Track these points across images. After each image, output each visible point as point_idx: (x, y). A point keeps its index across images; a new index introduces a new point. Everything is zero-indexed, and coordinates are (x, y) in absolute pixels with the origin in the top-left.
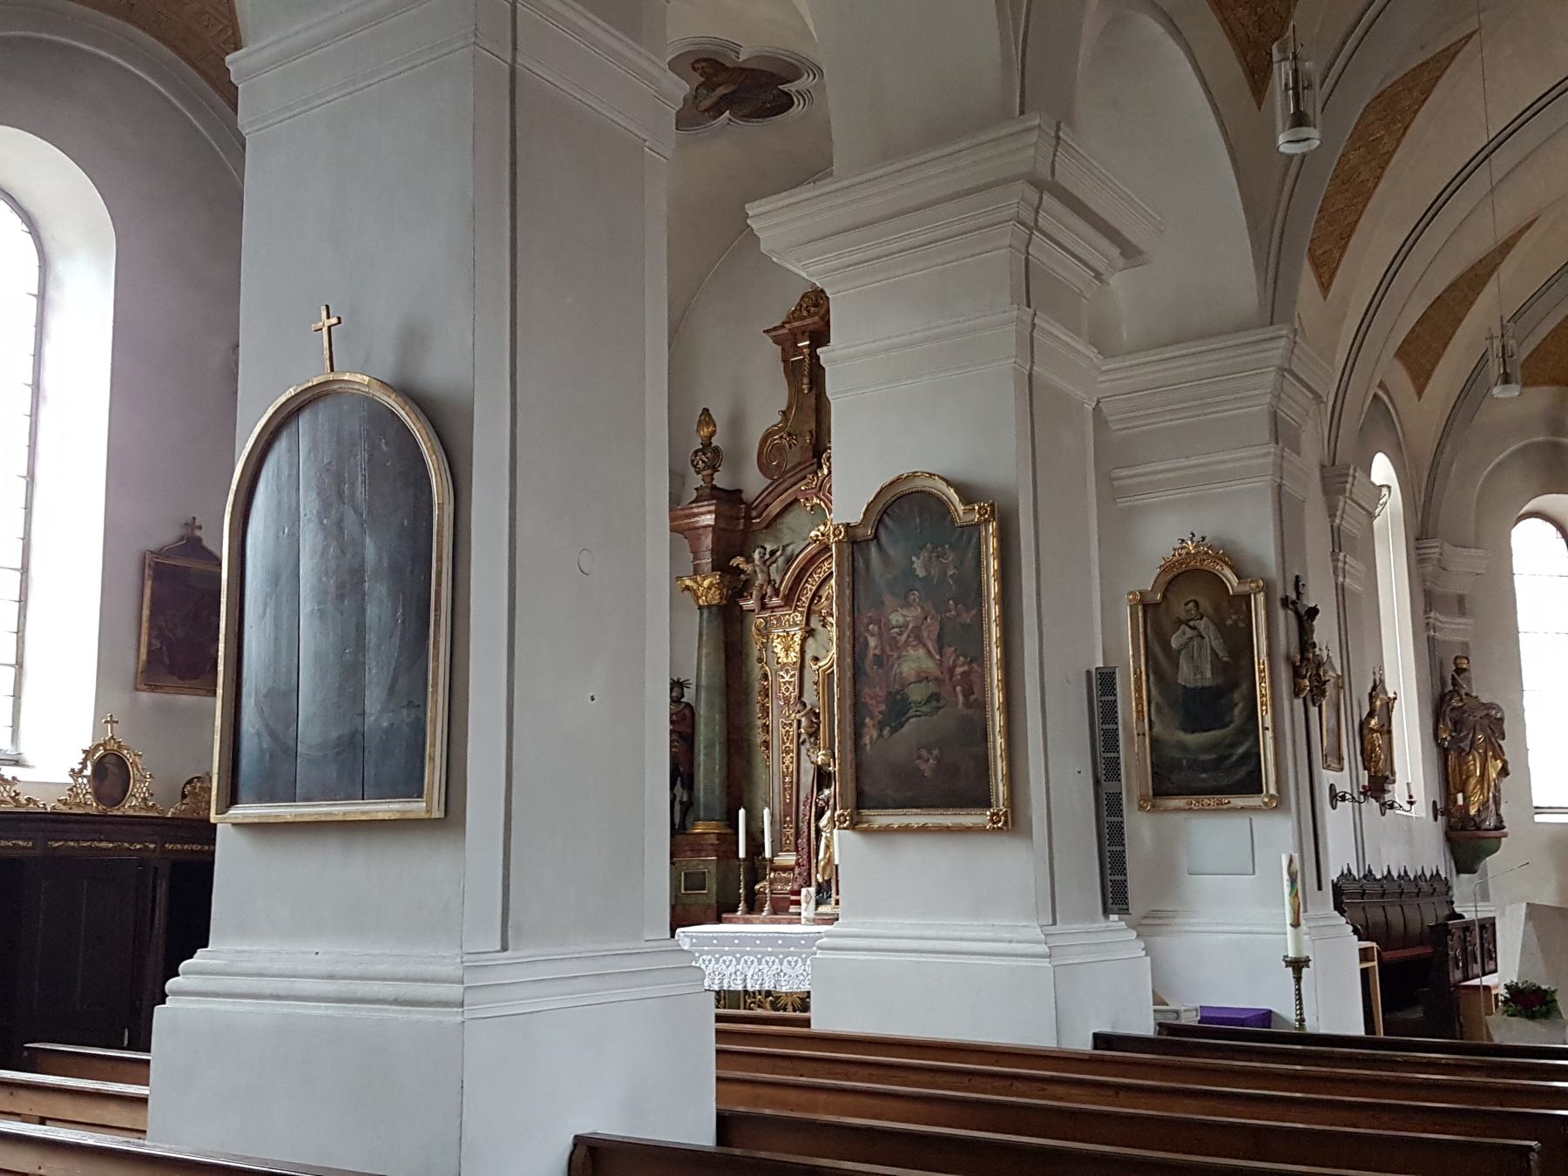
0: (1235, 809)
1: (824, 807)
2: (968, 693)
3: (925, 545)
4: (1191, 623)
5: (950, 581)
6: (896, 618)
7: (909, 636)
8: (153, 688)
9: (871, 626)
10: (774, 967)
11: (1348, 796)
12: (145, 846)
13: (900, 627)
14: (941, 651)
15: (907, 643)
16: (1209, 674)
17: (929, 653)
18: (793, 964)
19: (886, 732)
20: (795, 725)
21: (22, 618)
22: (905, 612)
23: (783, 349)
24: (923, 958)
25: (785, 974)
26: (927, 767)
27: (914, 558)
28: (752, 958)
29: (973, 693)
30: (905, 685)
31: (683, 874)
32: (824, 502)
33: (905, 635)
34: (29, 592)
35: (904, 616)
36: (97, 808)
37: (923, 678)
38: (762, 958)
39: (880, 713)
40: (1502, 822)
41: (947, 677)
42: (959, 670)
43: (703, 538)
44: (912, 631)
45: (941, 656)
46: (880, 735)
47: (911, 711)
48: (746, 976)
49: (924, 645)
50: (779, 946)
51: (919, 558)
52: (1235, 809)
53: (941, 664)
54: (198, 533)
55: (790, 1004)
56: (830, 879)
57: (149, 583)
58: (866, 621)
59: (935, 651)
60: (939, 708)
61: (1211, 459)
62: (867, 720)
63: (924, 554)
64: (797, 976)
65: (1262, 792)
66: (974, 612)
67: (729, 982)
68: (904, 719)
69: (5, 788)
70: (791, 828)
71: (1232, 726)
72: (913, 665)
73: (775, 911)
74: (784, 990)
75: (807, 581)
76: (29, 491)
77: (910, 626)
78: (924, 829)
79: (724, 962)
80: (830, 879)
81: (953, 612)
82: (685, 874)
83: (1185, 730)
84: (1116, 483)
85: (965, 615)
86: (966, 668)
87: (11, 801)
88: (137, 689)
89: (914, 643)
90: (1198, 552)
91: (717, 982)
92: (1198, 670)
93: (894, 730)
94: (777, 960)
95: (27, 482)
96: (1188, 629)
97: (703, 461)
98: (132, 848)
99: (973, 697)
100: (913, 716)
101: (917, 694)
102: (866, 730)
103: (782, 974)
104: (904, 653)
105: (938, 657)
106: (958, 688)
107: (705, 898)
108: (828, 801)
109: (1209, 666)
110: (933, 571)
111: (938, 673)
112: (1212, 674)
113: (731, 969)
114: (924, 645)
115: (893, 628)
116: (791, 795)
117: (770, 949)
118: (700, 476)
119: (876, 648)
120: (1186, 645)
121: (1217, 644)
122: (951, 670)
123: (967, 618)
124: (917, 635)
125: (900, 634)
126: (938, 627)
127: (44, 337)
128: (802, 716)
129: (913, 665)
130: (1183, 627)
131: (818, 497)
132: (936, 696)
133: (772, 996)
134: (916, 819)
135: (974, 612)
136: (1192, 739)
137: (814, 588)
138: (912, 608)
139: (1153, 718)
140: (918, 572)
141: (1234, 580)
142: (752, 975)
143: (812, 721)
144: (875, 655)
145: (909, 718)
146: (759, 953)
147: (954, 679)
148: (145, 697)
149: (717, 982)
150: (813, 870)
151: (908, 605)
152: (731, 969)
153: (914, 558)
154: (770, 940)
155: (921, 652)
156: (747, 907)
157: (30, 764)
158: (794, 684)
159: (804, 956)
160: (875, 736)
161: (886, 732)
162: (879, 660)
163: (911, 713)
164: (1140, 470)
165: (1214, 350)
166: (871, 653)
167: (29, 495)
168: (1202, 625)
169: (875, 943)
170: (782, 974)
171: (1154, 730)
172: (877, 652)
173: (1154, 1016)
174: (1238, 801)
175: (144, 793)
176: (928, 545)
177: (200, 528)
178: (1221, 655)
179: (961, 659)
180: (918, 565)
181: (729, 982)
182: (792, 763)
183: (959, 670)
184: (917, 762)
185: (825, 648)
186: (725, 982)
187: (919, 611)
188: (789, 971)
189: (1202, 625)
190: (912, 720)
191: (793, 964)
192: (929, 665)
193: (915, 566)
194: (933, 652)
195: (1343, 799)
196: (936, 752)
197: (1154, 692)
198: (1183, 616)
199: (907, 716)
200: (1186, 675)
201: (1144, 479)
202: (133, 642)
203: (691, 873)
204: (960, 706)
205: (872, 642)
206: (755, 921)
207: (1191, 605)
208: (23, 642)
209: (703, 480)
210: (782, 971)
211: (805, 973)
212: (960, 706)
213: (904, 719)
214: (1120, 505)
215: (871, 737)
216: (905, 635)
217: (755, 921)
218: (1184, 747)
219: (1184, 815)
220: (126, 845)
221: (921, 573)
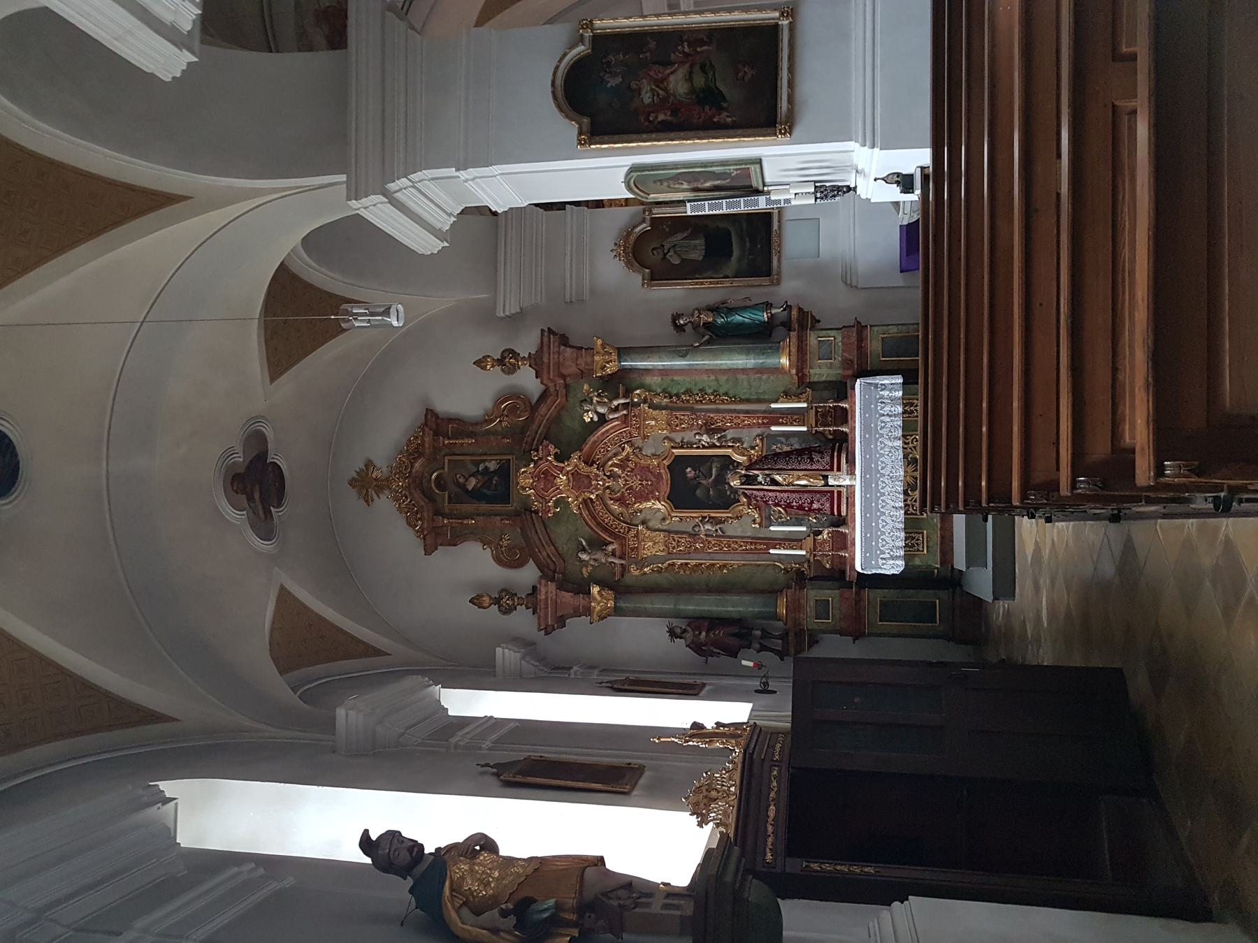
0: (780, 227)
1: (771, 478)
2: (702, 43)
3: (601, 77)
4: (666, 252)
5: (627, 57)
6: (647, 98)
7: (661, 89)
9: (651, 119)
10: (887, 539)
11: (764, 680)
13: (654, 95)
14: (672, 64)
15: (665, 90)
16: (698, 242)
17: (672, 73)
18: (884, 465)
19: (725, 105)
20: (710, 539)
22: (643, 93)
23: (441, 545)
24: (878, 62)
25: (891, 472)
26: (749, 72)
27: (609, 85)
28: (880, 502)
29: (703, 39)
30: (693, 91)
31: (819, 361)
32: (553, 497)
33: (660, 92)
35: (646, 93)
37: (689, 77)
38: (880, 492)
39: (710, 109)
41: (690, 58)
42: (687, 50)
43: (564, 600)
44: (657, 86)
45: (676, 63)
46: (726, 109)
47: (711, 85)
48: (893, 507)
49: (668, 75)
50: (871, 456)
51: (609, 82)
52: (780, 227)
53: (682, 63)
55: (912, 474)
56: (822, 476)
58: (647, 123)
59: (672, 68)
60: (711, 64)
61: (569, 254)
62: (715, 120)
63: (607, 77)
64: (892, 462)
65: (770, 213)
66: (649, 39)
67: (898, 522)
68: (716, 91)
70: (785, 544)
71: (730, 229)
72: (680, 83)
73: (845, 548)
74: (902, 473)
75: (606, 524)
77: (654, 87)
78: (791, 70)
79: (883, 527)
80: (822, 476)
81: (648, 54)
82: (816, 619)
83: (731, 256)
84: (573, 300)
85: (651, 46)
86: (685, 44)
89: (665, 83)
90: (623, 245)
91: (898, 534)
92: (695, 248)
93: (724, 99)
94: (882, 556)
96: (670, 254)
97: (508, 600)
99: (705, 39)
100: (715, 83)
101: (699, 81)
102: (722, 121)
103: (891, 474)
104: (672, 92)
105: (677, 65)
106: (698, 49)
107: (835, 600)
108: (767, 475)
109: (693, 242)
110: (619, 71)
111: (687, 66)
112: (697, 239)
113: (888, 520)
114: (668, 75)
115: (653, 101)
116: (761, 544)
117: (873, 485)
118: (521, 367)
119: (666, 114)
120: (679, 255)
121: (680, 236)
122: (687, 55)
123: (653, 45)
124: (660, 82)
125: (658, 94)
126: (657, 66)
128: (704, 528)
129: (680, 83)
130: (667, 256)
131: (549, 502)
132: (703, 68)
133: (907, 490)
135: (649, 39)
136: (736, 253)
137: (612, 517)
138: (642, 86)
139: (722, 276)
140: (617, 82)
141: (644, 225)
142: (893, 501)
143: (708, 521)
144: (670, 115)
145: (716, 87)
146: (876, 495)
147: (692, 53)
149: (898, 534)
150: (816, 488)
151: (639, 90)
152: (888, 520)
153: (609, 85)
154: (867, 526)
155: (672, 78)
156: (842, 525)
158: (680, 538)
159: (879, 495)
160: (726, 114)
161: (725, 105)
162: (674, 112)
163: (712, 85)
164: (568, 285)
165: (506, 235)
166: (669, 118)
168: (667, 246)
169: (869, 100)
170: (890, 434)
171: (730, 276)
172: (669, 114)
173: (908, 201)
174: (775, 226)
176: (601, 74)
178: (686, 235)
179: (679, 48)
180: (613, 82)
181: (898, 522)
182: (737, 542)
183: (687, 50)
184: (746, 80)
185: (656, 513)
186: (897, 544)
187: (644, 80)
188: (889, 468)
189: (667, 246)
190: (718, 84)
191: (884, 465)
192: (681, 73)
193: (613, 85)
194: (673, 69)
195: (766, 684)
196: (740, 66)
197: (705, 275)
198: (661, 256)
199: (714, 87)
200: (697, 255)
201: (574, 238)
203: (816, 614)
204: (711, 48)
205: (661, 117)
206: (853, 537)
207: (655, 252)
209: (521, 605)
210: (889, 475)
211: (890, 455)
212: (711, 48)
213: (716, 91)
214: (588, 297)
215: (728, 116)
216: (660, 92)
217: (853, 537)
218: (740, 260)
219: (783, 258)
220: (772, 795)
221: (619, 80)
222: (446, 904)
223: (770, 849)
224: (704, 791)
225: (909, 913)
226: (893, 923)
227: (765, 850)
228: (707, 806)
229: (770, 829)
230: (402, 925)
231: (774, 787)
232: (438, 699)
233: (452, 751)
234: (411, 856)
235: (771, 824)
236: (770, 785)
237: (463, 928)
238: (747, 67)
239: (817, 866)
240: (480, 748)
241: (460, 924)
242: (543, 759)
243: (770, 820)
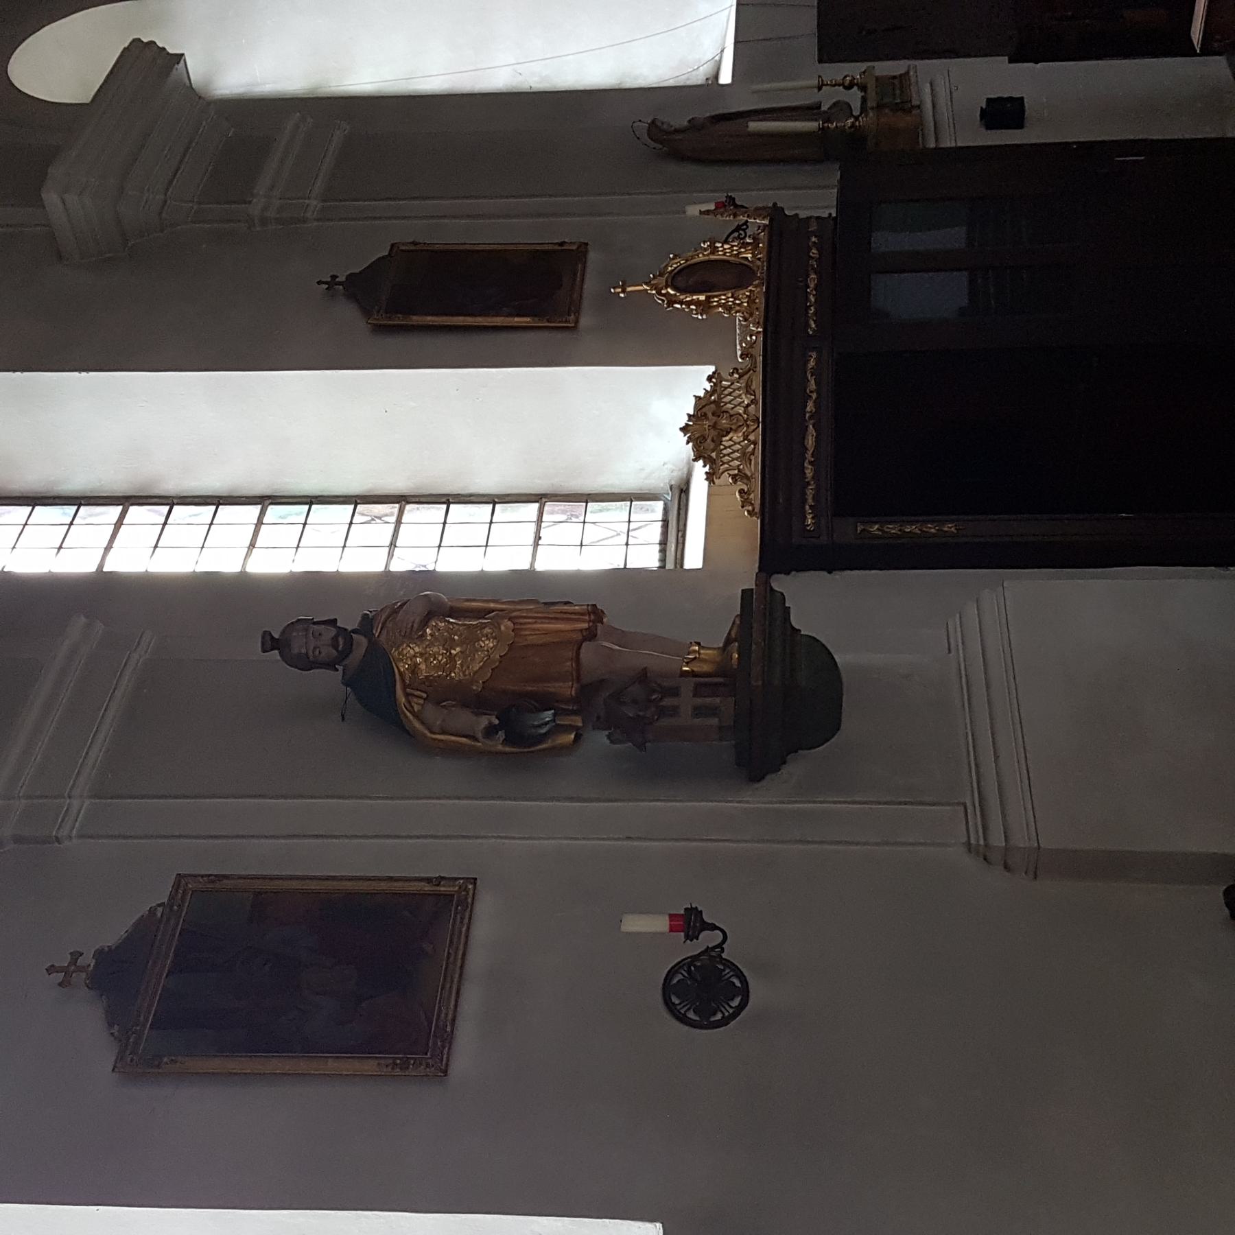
8: (574, 308)
12: (810, 418)
21: (472, 499)
34: (434, 492)
36: (756, 286)
40: (764, 208)
54: (88, 960)
57: (416, 320)
69: (726, 388)
76: (283, 500)
87: (746, 377)
88: (574, 328)
95: (272, 504)
98: (814, 396)
127: (52, 494)
134: (457, 247)
148: (584, 321)
157: (685, 471)
167: (295, 500)
175: (733, 246)
177: (76, 955)
202: (503, 337)
208: (508, 495)
220: (810, 406)
222: (405, 715)
223: (811, 507)
224: (710, 415)
225: (1004, 621)
226: (994, 743)
227: (804, 508)
228: (717, 442)
229: (809, 472)
230: (343, 719)
231: (811, 392)
232: (188, 84)
233: (258, 229)
234: (337, 650)
235: (810, 463)
236: (805, 391)
237: (435, 739)
238: (955, 532)
239: (878, 529)
240: (305, 221)
241: (429, 735)
242: (418, 247)
243: (809, 455)
